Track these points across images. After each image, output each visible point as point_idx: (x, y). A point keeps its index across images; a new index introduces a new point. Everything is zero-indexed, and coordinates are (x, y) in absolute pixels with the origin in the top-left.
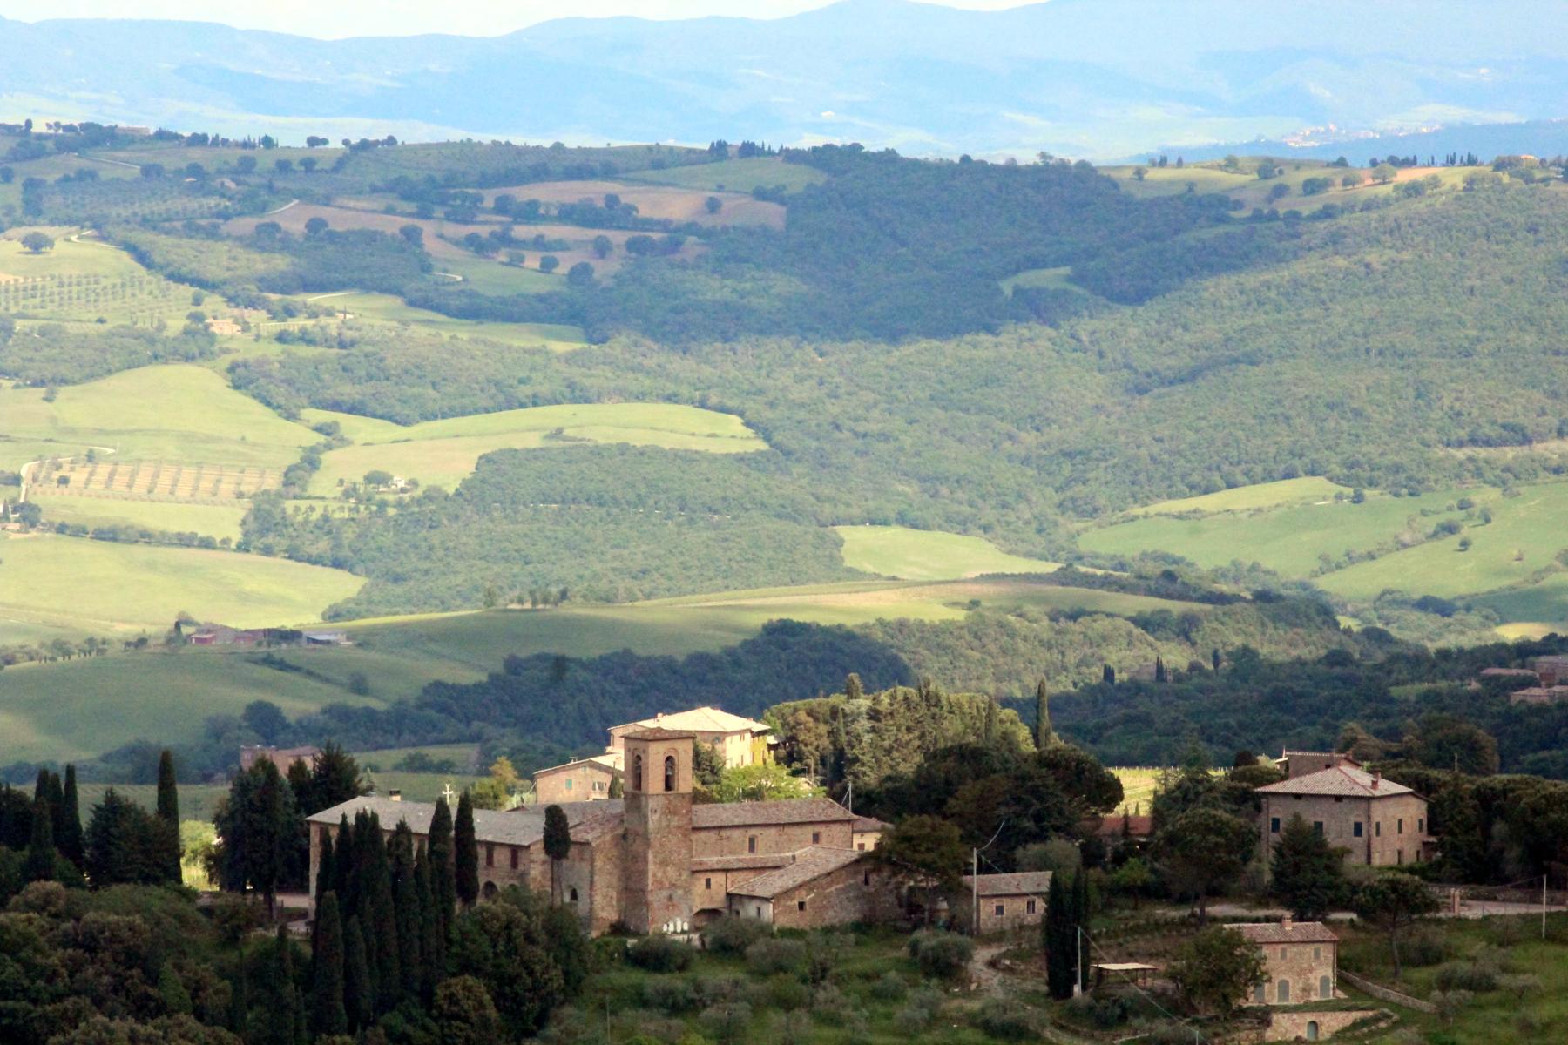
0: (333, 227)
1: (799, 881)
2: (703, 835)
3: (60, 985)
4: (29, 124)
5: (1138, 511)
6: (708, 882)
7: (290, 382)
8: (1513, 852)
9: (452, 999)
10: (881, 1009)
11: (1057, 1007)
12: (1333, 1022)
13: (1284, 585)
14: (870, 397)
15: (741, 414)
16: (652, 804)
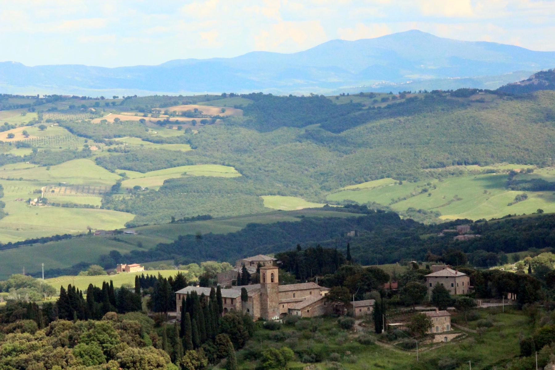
0: (121, 120)
1: (307, 304)
2: (281, 294)
3: (118, 340)
4: (38, 95)
5: (342, 189)
6: (283, 306)
7: (112, 163)
8: (494, 290)
9: (220, 339)
10: (332, 338)
11: (379, 336)
12: (451, 337)
13: (383, 207)
14: (268, 161)
15: (234, 166)
16: (268, 286)
